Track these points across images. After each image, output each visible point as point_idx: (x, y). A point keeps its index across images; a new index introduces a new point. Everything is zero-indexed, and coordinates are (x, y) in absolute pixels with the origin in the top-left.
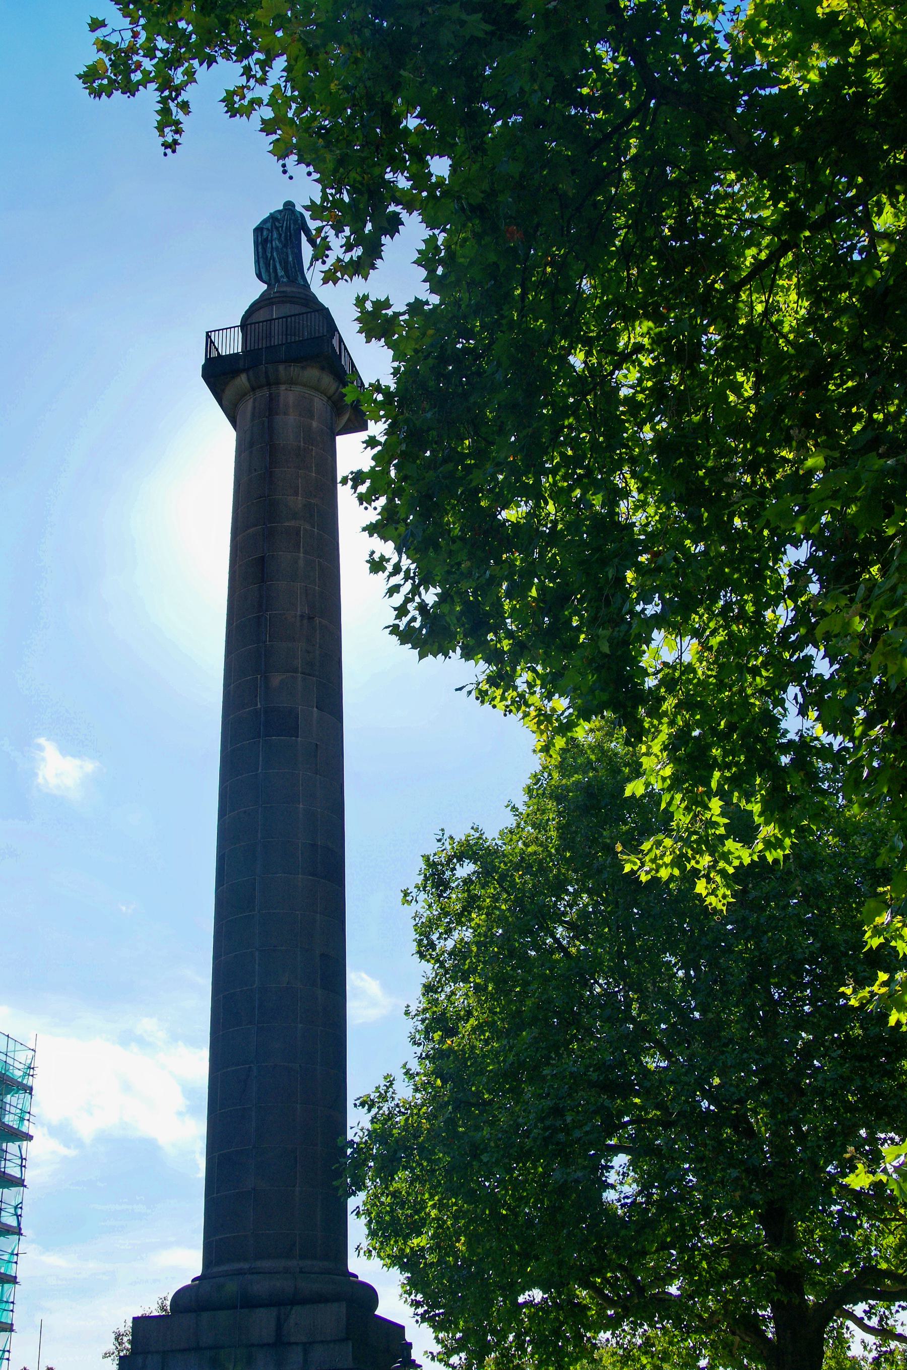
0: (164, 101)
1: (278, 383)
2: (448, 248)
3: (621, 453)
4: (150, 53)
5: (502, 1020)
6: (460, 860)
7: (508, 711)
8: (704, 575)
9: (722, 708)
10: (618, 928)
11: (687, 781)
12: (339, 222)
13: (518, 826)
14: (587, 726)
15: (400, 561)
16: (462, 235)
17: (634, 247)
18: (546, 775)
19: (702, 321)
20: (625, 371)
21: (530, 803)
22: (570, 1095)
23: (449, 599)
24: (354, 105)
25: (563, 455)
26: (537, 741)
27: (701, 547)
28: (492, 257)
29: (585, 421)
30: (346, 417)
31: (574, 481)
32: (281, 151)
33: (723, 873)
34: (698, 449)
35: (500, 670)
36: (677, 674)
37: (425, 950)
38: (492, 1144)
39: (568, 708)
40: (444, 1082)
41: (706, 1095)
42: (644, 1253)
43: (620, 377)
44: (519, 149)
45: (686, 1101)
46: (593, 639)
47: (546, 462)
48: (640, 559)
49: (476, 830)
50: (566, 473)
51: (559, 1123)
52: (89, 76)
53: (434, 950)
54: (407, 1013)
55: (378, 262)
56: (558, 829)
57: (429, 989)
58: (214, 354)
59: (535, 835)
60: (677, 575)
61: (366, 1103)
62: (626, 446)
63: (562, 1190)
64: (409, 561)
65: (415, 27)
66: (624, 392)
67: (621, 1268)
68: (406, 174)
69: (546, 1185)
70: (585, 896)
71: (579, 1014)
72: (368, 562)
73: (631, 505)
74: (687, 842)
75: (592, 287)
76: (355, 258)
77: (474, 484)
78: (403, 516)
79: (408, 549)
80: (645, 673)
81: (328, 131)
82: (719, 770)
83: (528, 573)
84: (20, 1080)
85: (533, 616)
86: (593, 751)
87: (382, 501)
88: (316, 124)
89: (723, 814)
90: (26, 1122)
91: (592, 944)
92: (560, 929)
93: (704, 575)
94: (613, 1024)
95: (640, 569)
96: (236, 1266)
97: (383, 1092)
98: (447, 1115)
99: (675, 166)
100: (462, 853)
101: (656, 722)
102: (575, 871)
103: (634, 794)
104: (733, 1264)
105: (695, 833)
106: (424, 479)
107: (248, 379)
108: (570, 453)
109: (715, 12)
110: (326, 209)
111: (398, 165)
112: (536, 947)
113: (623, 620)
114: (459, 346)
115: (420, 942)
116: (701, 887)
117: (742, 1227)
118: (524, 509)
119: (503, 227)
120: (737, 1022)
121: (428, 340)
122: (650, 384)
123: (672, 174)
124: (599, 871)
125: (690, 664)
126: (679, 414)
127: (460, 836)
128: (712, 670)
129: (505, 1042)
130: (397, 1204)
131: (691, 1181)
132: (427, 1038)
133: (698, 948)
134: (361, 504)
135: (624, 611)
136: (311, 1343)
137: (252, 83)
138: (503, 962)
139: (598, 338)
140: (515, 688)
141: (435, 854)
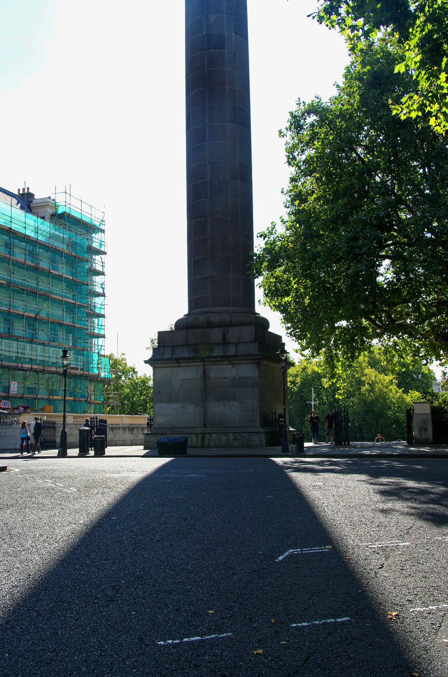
5: (329, 195)
6: (309, 114)
13: (340, 95)
22: (362, 231)
37: (291, 160)
40: (300, 226)
49: (318, 98)
57: (293, 180)
74: (426, 97)
84: (98, 226)
90: (103, 246)
97: (270, 230)
98: (301, 242)
100: (309, 110)
103: (399, 72)
105: (431, 92)
112: (348, 158)
115: (288, 157)
116: (432, 121)
129: (330, 205)
130: (278, 282)
132: (293, 204)
136: (239, 343)
141: (296, 111)
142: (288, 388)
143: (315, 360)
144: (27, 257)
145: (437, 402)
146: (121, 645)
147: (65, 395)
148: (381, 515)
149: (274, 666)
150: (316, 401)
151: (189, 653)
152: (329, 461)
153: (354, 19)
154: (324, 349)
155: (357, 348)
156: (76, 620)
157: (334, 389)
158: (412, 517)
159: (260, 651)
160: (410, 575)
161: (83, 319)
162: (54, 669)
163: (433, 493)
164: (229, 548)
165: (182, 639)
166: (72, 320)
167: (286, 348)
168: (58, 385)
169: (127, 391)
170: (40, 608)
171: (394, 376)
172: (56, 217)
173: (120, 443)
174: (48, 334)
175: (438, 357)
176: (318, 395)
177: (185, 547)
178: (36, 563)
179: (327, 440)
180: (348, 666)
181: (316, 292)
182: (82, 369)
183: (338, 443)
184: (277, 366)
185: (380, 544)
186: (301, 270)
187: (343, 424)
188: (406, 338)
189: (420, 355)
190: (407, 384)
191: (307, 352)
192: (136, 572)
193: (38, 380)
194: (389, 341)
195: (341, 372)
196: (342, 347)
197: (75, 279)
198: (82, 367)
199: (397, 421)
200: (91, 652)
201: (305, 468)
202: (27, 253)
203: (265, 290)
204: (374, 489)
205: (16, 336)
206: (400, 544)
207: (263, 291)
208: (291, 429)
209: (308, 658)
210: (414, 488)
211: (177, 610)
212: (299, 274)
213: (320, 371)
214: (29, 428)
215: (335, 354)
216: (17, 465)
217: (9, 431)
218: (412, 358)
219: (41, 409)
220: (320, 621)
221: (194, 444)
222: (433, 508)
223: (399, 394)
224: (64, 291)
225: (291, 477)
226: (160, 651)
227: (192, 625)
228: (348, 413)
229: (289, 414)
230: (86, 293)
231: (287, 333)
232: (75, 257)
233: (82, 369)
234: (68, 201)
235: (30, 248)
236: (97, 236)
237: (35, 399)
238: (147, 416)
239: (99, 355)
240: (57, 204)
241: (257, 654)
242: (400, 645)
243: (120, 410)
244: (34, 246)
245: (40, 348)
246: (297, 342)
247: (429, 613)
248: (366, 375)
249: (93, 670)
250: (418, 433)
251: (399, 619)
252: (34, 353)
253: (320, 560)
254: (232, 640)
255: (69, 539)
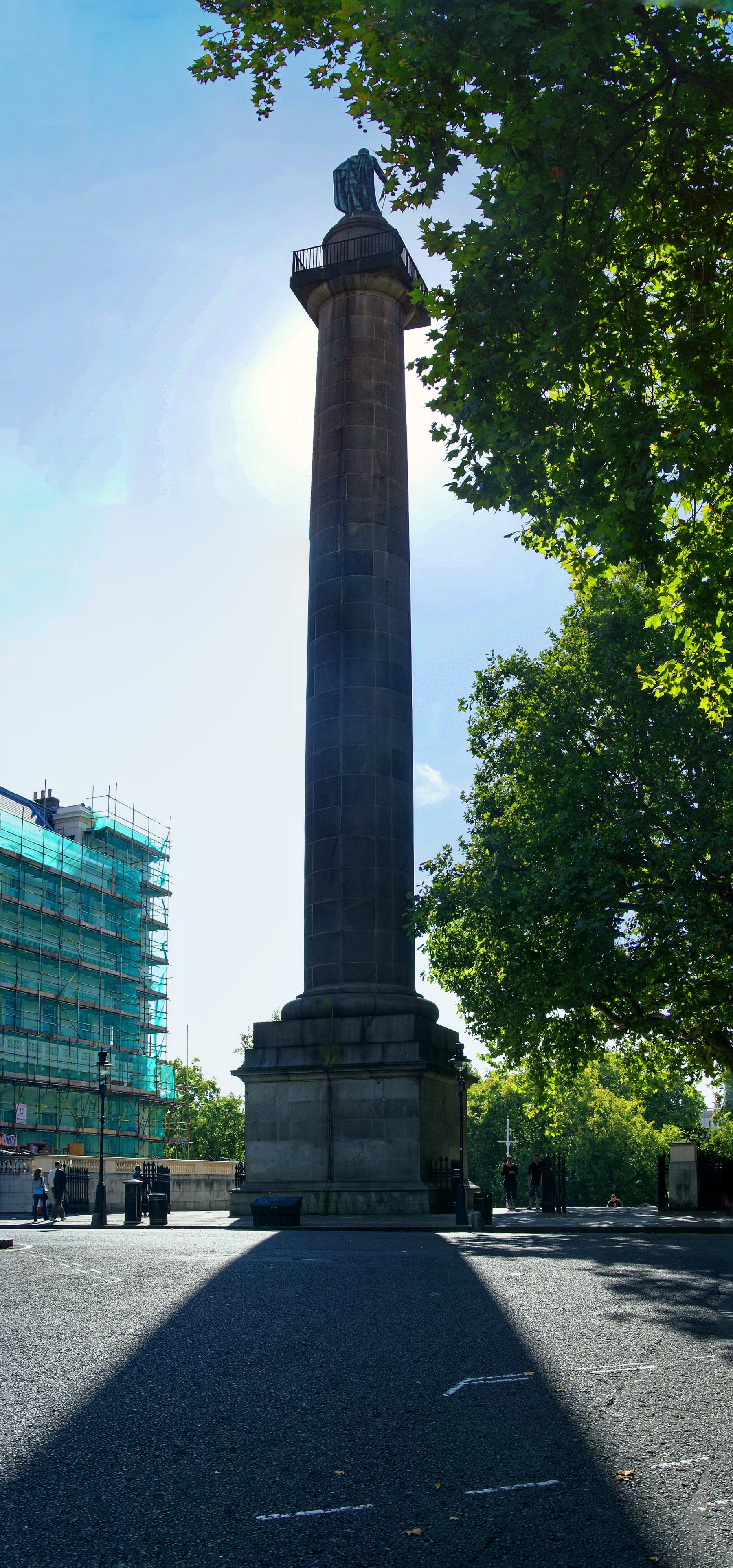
0: (259, 80)
1: (354, 289)
2: (500, 183)
3: (647, 349)
4: (248, 47)
5: (539, 804)
6: (507, 675)
7: (548, 555)
8: (715, 451)
9: (727, 560)
10: (635, 734)
11: (696, 618)
12: (406, 163)
13: (556, 649)
14: (615, 569)
15: (458, 431)
16: (512, 173)
17: (659, 187)
18: (579, 608)
19: (716, 249)
20: (651, 284)
21: (566, 630)
22: (592, 864)
23: (499, 462)
24: (419, 76)
25: (598, 348)
26: (572, 580)
27: (714, 428)
28: (538, 191)
29: (616, 321)
30: (412, 315)
31: (607, 369)
32: (357, 112)
33: (722, 693)
34: (712, 349)
35: (542, 521)
36: (691, 530)
38: (529, 900)
39: (599, 554)
41: (699, 867)
42: (644, 985)
43: (647, 288)
44: (560, 109)
45: (684, 872)
46: (622, 498)
47: (583, 353)
48: (662, 435)
49: (521, 652)
50: (601, 363)
51: (582, 885)
52: (199, 69)
53: (485, 747)
54: (462, 797)
55: (440, 194)
56: (588, 653)
57: (480, 778)
58: (300, 269)
59: (569, 657)
60: (693, 450)
61: (429, 867)
62: (652, 343)
63: (583, 936)
64: (466, 431)
65: (471, 19)
66: (650, 300)
67: (626, 995)
68: (463, 126)
69: (571, 932)
70: (609, 707)
71: (602, 801)
72: (430, 431)
73: (655, 391)
74: (694, 667)
75: (623, 216)
76: (420, 191)
77: (521, 369)
78: (461, 394)
79: (465, 421)
80: (664, 528)
81: (397, 95)
82: (723, 610)
83: (568, 442)
85: (571, 478)
86: (619, 590)
87: (443, 382)
88: (387, 90)
89: (724, 646)
91: (614, 746)
92: (588, 733)
93: (715, 451)
94: (629, 810)
95: (661, 442)
96: (330, 987)
98: (494, 877)
99: (693, 128)
100: (509, 670)
101: (672, 569)
102: (602, 687)
103: (652, 626)
104: (711, 994)
105: (702, 660)
106: (479, 364)
107: (329, 287)
108: (604, 346)
109: (725, 19)
110: (395, 153)
111: (456, 119)
113: (648, 484)
114: (509, 259)
115: (473, 742)
116: (704, 704)
117: (721, 968)
118: (564, 391)
119: (547, 167)
120: (727, 812)
121: (482, 254)
122: (672, 295)
123: (690, 134)
124: (622, 688)
125: (702, 523)
126: (697, 320)
127: (507, 656)
128: (720, 529)
129: (541, 822)
130: (454, 943)
131: (684, 932)
132: (478, 817)
133: (699, 753)
134: (425, 384)
135: (648, 476)
136: (387, 1043)
137: (333, 63)
138: (541, 758)
139: (628, 256)
140: (555, 536)
141: (486, 671)
142: (468, 1118)
143: (512, 1073)
144: (45, 900)
145: (706, 1144)
146: (198, 1519)
147: (102, 1126)
148: (612, 1324)
149: (439, 1552)
150: (514, 1140)
151: (305, 1533)
152: (532, 1238)
153: (581, 545)
154: (527, 1056)
155: (581, 1054)
156: (128, 1481)
157: (543, 1121)
158: (661, 1326)
159: (417, 1531)
160: (654, 1415)
161: (132, 1001)
162: (98, 1550)
163: (695, 1288)
164: (369, 1375)
165: (294, 1513)
166: (114, 1003)
167: (466, 1052)
168: (91, 1110)
169: (203, 1120)
170: (72, 1461)
171: (640, 1101)
172: (92, 836)
173: (192, 1205)
174: (76, 1026)
175: (710, 1072)
176: (517, 1130)
177: (297, 1373)
178: (63, 1393)
179: (530, 1204)
180: (552, 1551)
181: (517, 961)
182: (129, 1085)
183: (548, 1209)
184: (451, 1081)
185: (610, 1369)
186: (491, 924)
187: (557, 1178)
188: (660, 1039)
189: (682, 1067)
190: (660, 1113)
191: (500, 1060)
192: (220, 1410)
193: (60, 1102)
194: (633, 1044)
195: (554, 1092)
196: (557, 1052)
197: (119, 936)
198: (129, 1081)
199: (642, 1174)
200: (152, 1528)
201: (493, 1249)
202: (45, 894)
203: (432, 956)
204: (603, 1283)
205: (26, 1030)
206: (641, 1368)
207: (429, 957)
208: (472, 1186)
209: (491, 1540)
210: (666, 1281)
211: (286, 1469)
212: (488, 930)
213: (520, 1092)
214: (46, 1180)
215: (546, 1064)
216: (28, 1239)
217: (15, 1184)
218: (669, 1073)
219: (64, 1149)
220: (512, 1485)
221: (312, 1209)
222: (693, 1312)
223: (646, 1130)
224: (103, 956)
225: (471, 1264)
226: (260, 1529)
227: (310, 1492)
228: (564, 1160)
229: (469, 1162)
230: (138, 958)
231: (468, 1028)
232: (121, 900)
233: (129, 1085)
234: (112, 810)
235: (50, 886)
236: (157, 867)
237: (55, 1132)
238: (235, 1162)
239: (158, 1061)
240: (95, 815)
241: (412, 1534)
242: (633, 1518)
243: (191, 1152)
244: (56, 882)
245: (62, 1048)
246: (484, 1043)
247: (680, 1470)
248: (595, 1098)
249: (158, 1554)
250: (675, 1193)
251: (634, 1480)
252: (54, 1057)
253: (514, 1394)
254: (373, 1514)
255: (112, 1358)
